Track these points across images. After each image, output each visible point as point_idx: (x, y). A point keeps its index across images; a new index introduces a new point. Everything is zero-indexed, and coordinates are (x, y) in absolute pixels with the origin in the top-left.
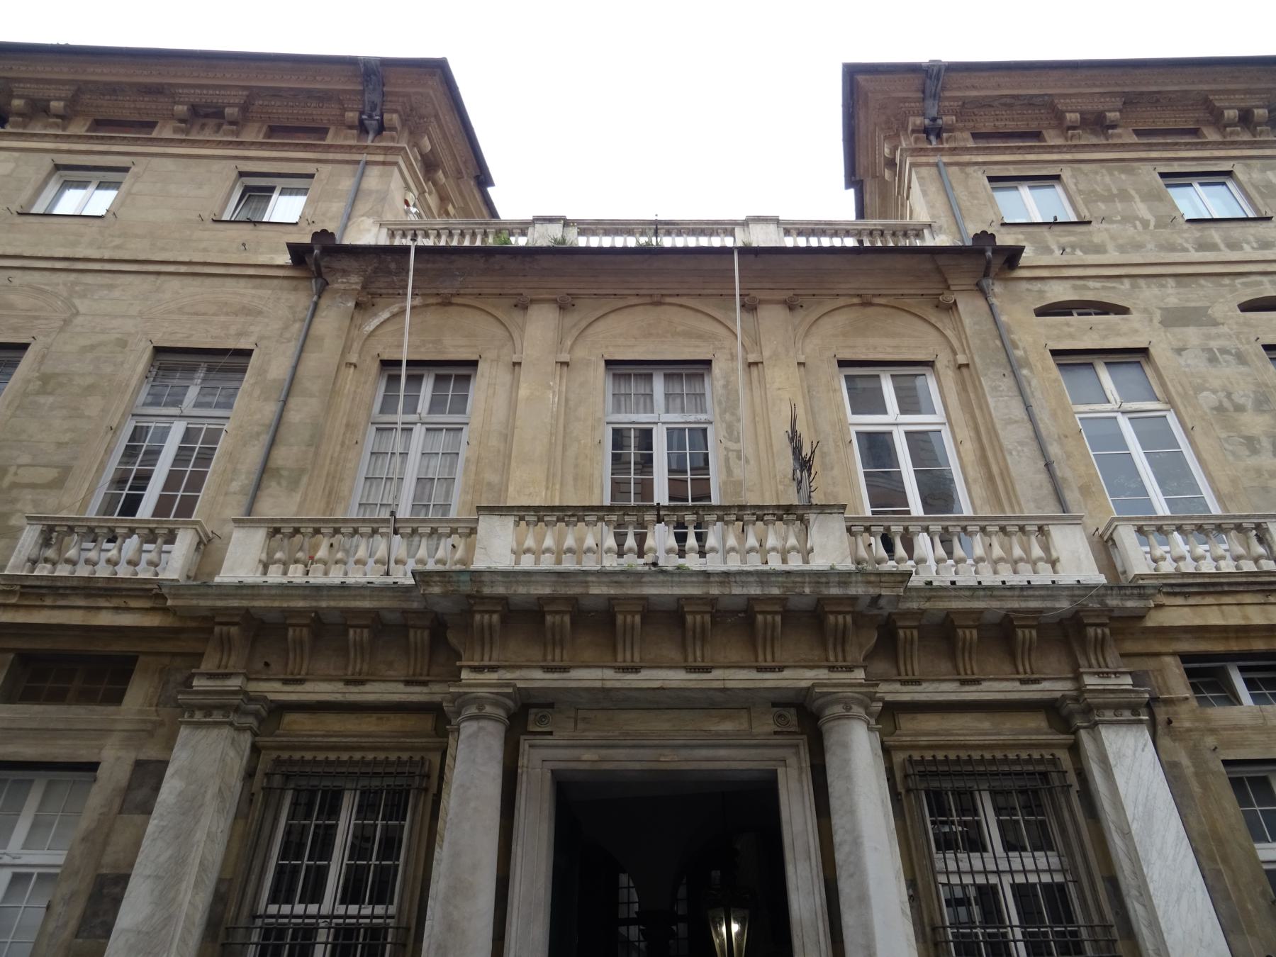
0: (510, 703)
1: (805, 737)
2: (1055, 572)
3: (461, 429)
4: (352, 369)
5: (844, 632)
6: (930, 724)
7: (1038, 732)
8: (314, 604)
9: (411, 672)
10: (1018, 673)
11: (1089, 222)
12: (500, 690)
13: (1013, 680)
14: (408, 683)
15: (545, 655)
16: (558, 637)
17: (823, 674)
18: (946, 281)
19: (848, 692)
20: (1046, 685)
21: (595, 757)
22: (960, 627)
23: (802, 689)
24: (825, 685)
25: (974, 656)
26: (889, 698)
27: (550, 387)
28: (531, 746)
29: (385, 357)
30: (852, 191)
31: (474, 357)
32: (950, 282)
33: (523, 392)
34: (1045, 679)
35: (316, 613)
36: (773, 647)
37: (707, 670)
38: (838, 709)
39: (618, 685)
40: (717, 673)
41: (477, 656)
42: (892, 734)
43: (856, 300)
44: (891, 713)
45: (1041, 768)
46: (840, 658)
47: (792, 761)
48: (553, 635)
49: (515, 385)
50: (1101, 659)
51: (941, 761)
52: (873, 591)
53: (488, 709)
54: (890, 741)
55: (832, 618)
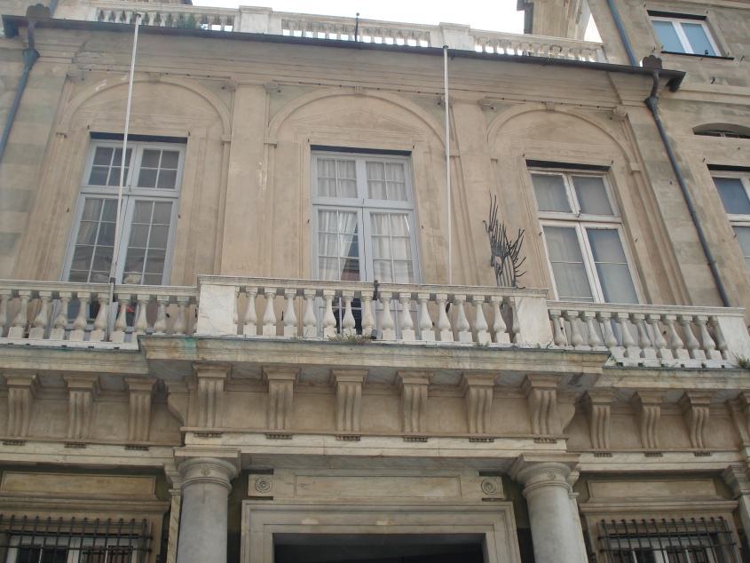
0: (233, 468)
1: (511, 503)
2: (724, 358)
3: (171, 203)
4: (62, 139)
5: (549, 407)
6: (618, 490)
7: (708, 498)
8: (36, 366)
9: (131, 437)
10: (693, 447)
11: (732, 59)
12: (222, 455)
13: (689, 452)
14: (129, 447)
15: (268, 423)
16: (280, 405)
17: (529, 445)
18: (618, 96)
19: (553, 462)
20: (715, 457)
21: (315, 522)
22: (646, 404)
23: (509, 459)
24: (533, 455)
25: (656, 431)
26: (585, 468)
27: (260, 167)
28: (252, 510)
29: (96, 129)
30: (522, 13)
31: (183, 135)
32: (622, 97)
33: (234, 169)
34: (714, 452)
35: (37, 376)
36: (483, 418)
37: (423, 439)
38: (544, 477)
39: (339, 452)
40: (432, 443)
41: (201, 423)
42: (586, 501)
43: (541, 107)
44: (587, 479)
45: (711, 529)
46: (544, 432)
47: (500, 526)
48: (277, 405)
49: (224, 164)
50: (544, 427)
51: (608, 525)
52: (576, 369)
53: (213, 474)
54: (586, 508)
55: (538, 393)
